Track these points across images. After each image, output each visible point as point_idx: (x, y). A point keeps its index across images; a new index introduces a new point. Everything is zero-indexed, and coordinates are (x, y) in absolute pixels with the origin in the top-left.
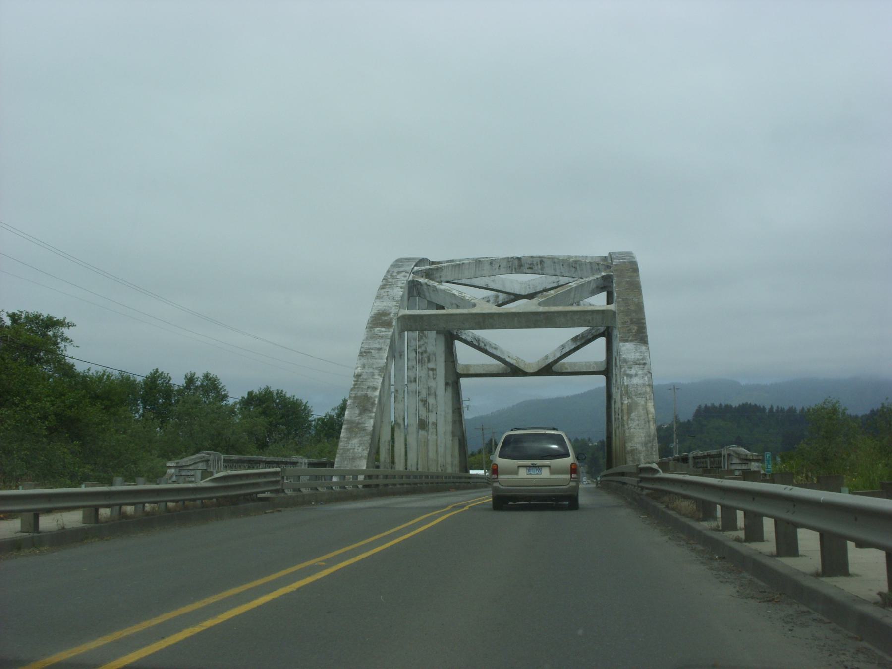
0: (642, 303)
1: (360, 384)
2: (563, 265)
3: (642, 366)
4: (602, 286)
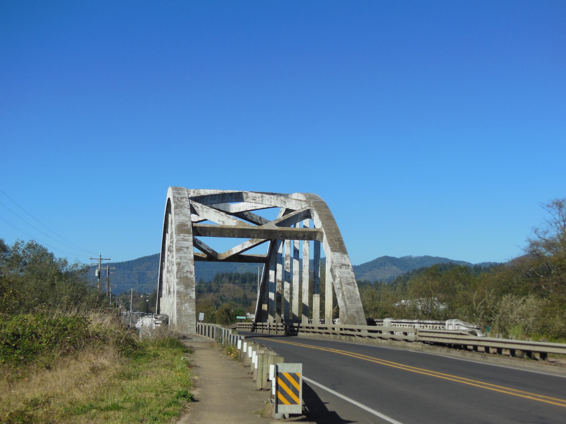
0: (338, 228)
1: (181, 270)
2: (277, 200)
3: (347, 267)
4: (306, 215)
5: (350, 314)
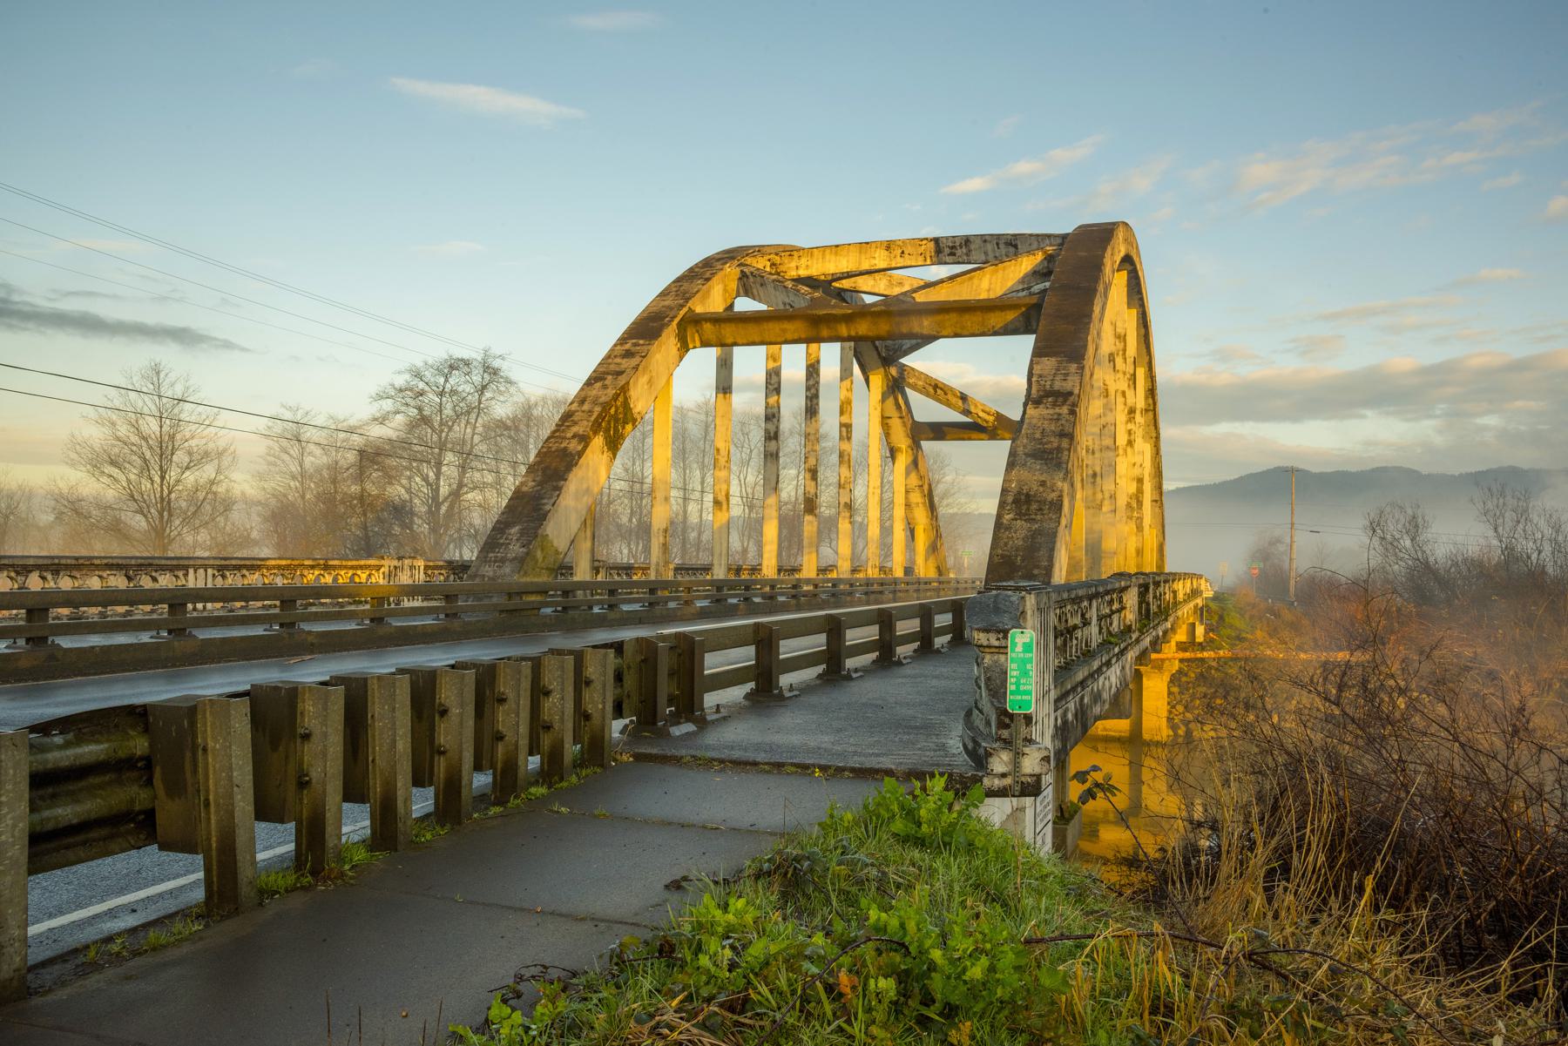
5: (1002, 556)
